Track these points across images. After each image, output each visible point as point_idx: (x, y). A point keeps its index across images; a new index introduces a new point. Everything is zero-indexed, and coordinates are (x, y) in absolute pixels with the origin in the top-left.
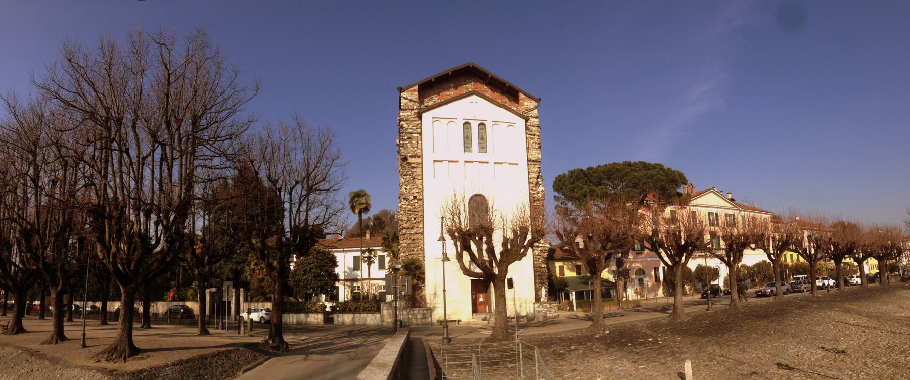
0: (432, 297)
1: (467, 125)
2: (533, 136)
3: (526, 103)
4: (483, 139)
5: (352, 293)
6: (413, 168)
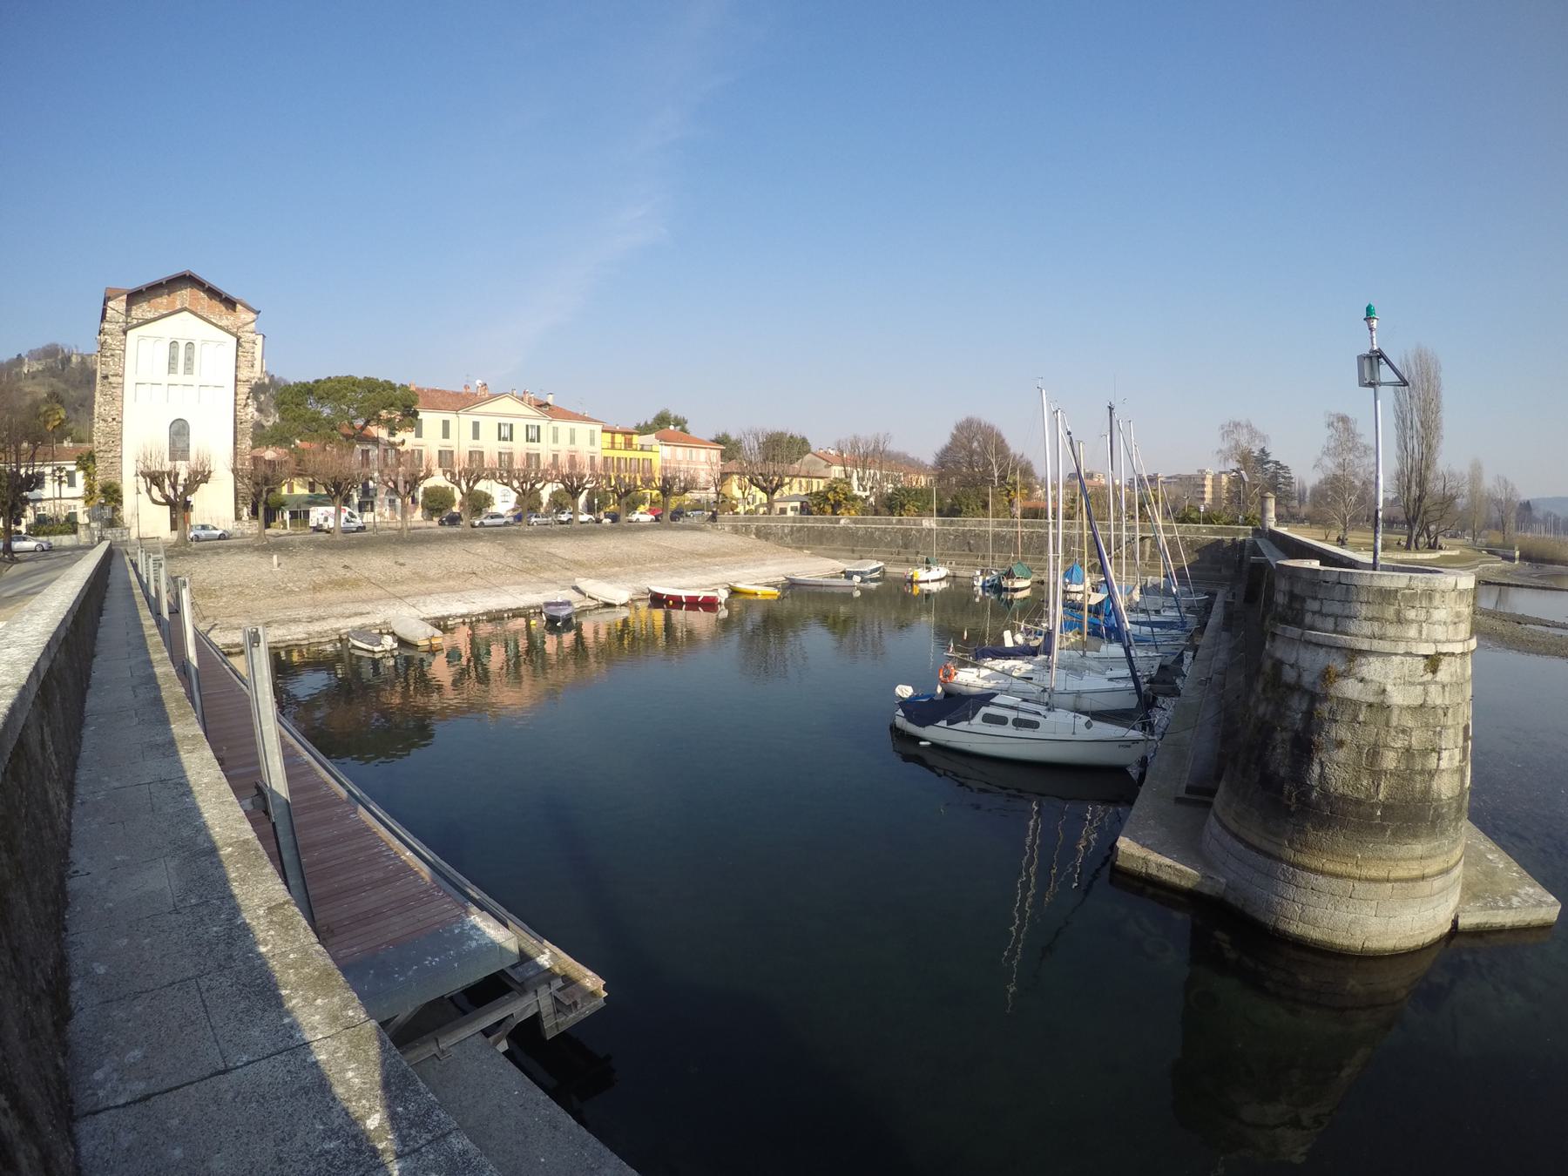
0: (130, 518)
1: (174, 344)
2: (246, 354)
3: (243, 316)
4: (189, 360)
5: (35, 514)
6: (114, 388)
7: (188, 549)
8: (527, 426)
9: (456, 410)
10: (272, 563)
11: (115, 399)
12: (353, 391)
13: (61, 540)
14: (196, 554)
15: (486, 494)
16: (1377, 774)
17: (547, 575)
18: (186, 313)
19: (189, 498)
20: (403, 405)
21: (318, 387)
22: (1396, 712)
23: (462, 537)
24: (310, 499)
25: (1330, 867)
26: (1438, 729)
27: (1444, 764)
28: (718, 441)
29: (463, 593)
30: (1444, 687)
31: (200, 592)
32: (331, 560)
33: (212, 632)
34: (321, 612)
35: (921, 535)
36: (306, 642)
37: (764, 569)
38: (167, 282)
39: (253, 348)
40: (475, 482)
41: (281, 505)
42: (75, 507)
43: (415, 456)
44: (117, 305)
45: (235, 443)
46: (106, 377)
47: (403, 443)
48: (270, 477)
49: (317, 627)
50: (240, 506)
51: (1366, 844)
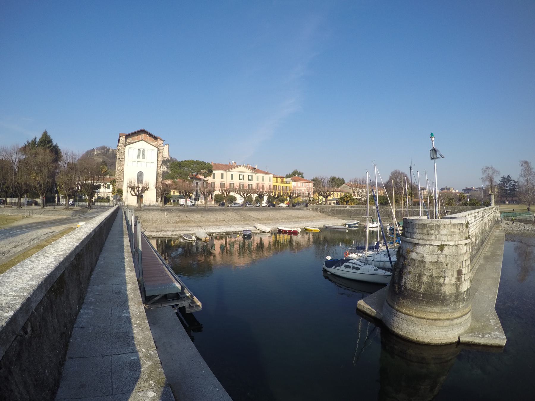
0: (125, 199)
1: (139, 150)
3: (159, 142)
4: (144, 154)
7: (141, 209)
8: (248, 175)
9: (226, 170)
10: (165, 214)
11: (122, 165)
12: (192, 165)
13: (105, 204)
14: (144, 211)
15: (234, 197)
16: (420, 283)
17: (247, 222)
18: (143, 141)
19: (142, 194)
20: (208, 169)
21: (182, 163)
22: (427, 263)
23: (224, 210)
24: (179, 196)
25: (406, 312)
26: (444, 270)
27: (446, 282)
28: (313, 180)
29: (220, 226)
30: (446, 256)
31: (144, 221)
32: (183, 215)
33: (145, 232)
34: (177, 229)
35: (372, 211)
36: (171, 237)
37: (319, 223)
38: (137, 132)
39: (163, 151)
40: (229, 193)
41: (170, 198)
42: (109, 195)
43: (213, 185)
44: (123, 139)
45: (157, 179)
46: (119, 159)
47: (208, 180)
48: (166, 189)
49: (175, 233)
50: (158, 198)
51: (417, 306)
